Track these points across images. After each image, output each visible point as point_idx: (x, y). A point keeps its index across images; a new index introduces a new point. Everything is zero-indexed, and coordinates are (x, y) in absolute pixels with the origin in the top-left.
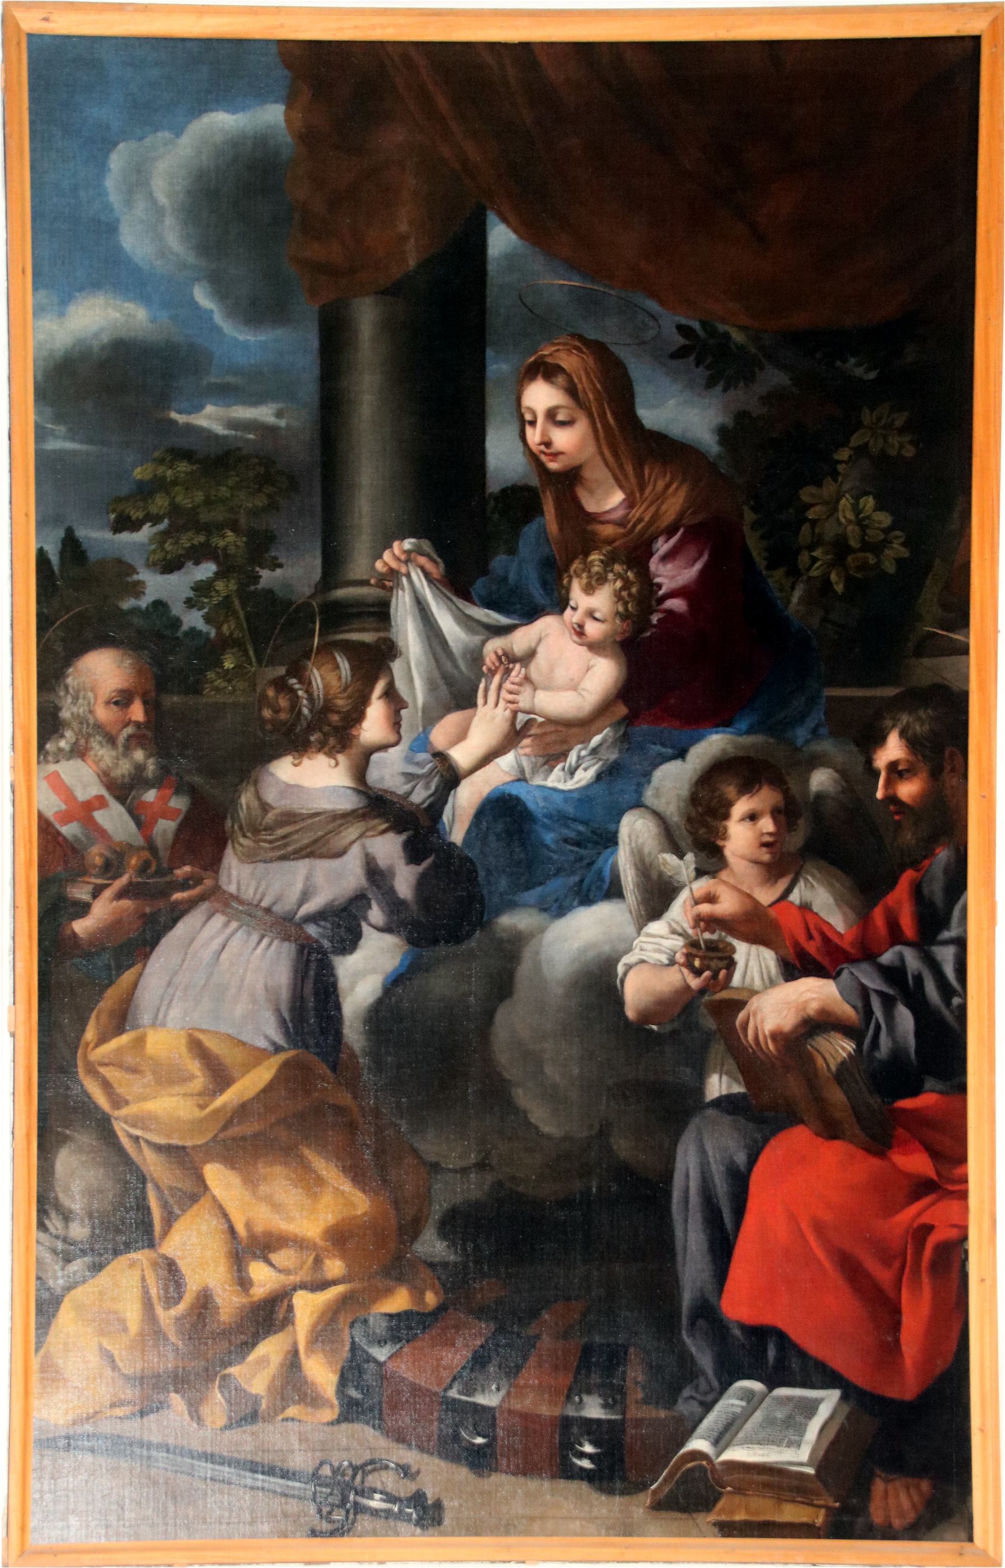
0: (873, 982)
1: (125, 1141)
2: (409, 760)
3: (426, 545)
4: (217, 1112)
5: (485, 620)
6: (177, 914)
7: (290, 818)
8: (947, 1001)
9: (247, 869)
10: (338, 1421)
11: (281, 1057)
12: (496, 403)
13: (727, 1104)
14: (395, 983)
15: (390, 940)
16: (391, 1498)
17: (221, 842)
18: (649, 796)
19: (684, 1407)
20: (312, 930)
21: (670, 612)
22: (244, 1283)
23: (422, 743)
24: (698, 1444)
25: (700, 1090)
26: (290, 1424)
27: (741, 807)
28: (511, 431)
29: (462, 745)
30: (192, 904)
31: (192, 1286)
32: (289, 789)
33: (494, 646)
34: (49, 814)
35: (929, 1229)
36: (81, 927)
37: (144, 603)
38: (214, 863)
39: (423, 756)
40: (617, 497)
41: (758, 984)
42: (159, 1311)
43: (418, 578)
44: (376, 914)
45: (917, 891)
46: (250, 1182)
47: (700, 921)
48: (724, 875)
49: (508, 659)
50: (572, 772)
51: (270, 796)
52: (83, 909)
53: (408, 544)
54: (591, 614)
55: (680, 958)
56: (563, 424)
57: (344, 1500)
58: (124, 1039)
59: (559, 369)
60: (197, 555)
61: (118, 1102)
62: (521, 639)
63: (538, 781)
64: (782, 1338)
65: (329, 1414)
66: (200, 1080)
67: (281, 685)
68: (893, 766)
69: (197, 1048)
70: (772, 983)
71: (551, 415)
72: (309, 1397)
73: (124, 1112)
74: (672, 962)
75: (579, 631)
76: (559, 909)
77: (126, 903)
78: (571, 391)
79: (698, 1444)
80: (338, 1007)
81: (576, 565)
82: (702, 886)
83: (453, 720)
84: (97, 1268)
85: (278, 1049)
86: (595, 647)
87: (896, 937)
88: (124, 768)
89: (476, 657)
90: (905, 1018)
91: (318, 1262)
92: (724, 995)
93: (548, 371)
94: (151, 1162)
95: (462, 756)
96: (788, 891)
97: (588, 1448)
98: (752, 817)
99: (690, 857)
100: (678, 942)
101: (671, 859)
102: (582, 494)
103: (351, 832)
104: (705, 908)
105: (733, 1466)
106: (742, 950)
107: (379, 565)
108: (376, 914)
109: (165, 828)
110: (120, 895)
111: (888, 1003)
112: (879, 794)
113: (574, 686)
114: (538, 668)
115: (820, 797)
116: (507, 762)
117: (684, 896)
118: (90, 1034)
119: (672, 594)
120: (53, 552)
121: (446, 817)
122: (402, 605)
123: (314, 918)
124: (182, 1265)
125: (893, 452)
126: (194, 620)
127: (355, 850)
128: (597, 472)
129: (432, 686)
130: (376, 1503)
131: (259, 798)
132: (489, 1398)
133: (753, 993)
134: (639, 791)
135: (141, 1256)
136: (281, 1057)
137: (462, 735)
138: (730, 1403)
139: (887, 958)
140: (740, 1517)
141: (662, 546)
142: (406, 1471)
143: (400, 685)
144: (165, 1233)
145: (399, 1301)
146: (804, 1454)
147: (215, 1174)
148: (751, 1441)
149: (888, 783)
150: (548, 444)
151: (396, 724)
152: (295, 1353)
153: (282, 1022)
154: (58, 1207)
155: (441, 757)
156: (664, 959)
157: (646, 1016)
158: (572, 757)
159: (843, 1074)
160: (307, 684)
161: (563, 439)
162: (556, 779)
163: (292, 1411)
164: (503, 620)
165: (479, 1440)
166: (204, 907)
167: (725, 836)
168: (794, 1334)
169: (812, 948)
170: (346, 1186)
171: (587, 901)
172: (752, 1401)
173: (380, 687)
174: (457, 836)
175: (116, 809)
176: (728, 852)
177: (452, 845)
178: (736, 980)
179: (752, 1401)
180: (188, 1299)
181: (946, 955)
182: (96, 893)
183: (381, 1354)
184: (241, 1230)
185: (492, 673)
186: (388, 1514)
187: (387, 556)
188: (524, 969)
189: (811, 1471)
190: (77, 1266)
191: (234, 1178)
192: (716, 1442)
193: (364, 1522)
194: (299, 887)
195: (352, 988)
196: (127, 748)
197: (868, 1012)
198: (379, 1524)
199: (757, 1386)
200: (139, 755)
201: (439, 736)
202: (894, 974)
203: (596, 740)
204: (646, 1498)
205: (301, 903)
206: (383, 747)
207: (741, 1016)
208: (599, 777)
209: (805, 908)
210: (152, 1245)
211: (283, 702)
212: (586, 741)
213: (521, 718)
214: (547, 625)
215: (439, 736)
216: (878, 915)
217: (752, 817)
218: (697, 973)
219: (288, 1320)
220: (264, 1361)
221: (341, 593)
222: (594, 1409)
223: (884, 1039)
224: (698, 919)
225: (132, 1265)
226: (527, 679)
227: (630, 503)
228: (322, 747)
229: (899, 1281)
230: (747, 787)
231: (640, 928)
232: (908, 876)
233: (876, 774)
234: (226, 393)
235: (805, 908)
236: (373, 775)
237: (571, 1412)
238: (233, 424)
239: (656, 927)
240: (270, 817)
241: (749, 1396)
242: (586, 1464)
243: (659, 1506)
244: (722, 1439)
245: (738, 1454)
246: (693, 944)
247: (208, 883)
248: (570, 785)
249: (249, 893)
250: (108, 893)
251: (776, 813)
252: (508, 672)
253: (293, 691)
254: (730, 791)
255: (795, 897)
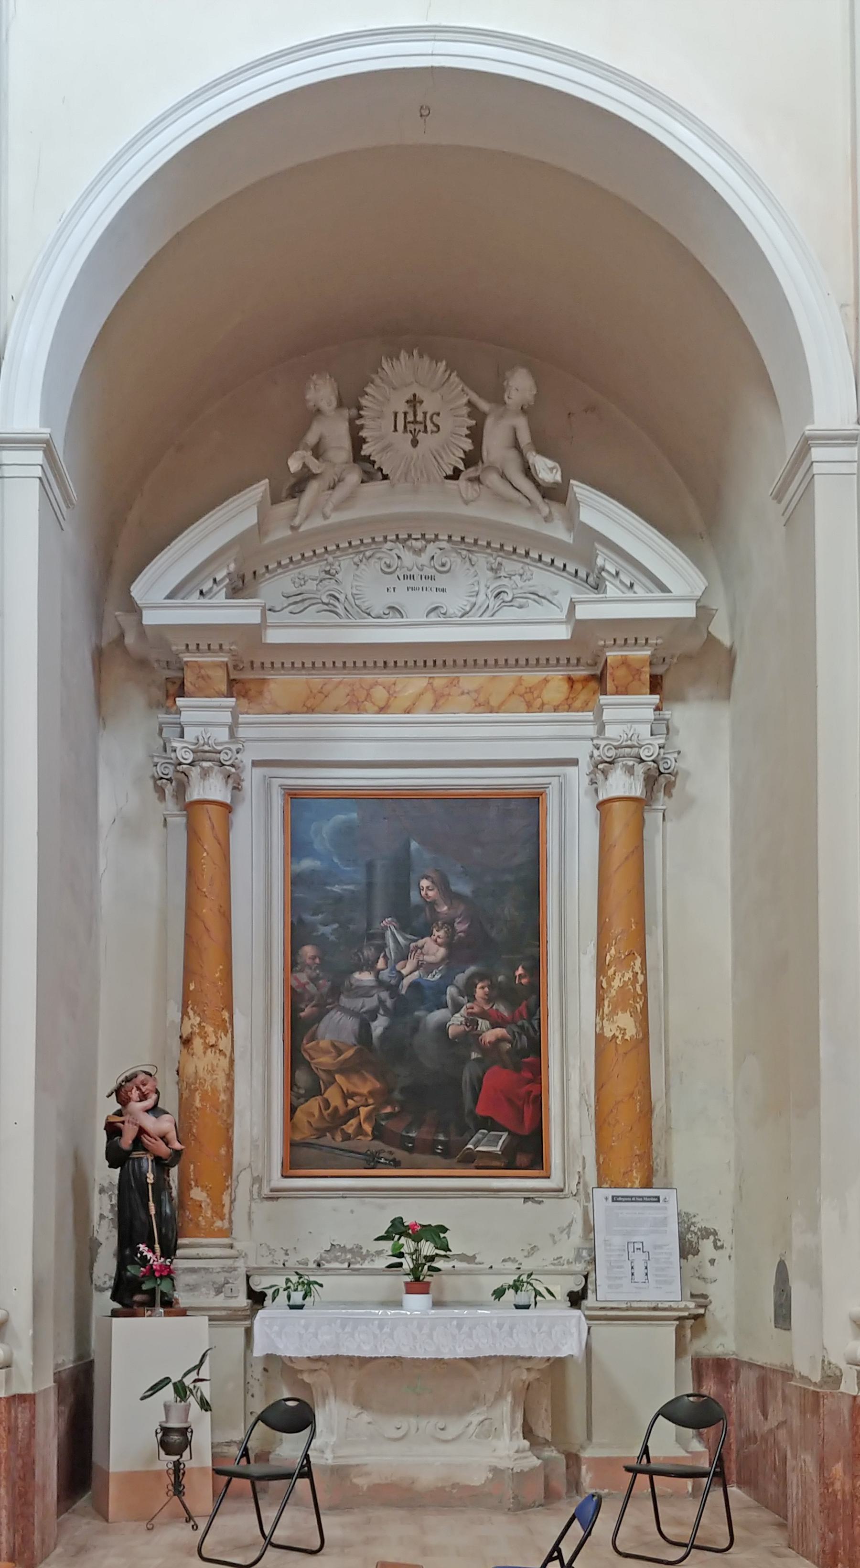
0: (516, 1030)
1: (314, 1068)
2: (389, 973)
3: (395, 920)
4: (338, 1062)
5: (40, 1436)
6: (328, 1011)
7: (358, 987)
8: (536, 1034)
9: (346, 1000)
10: (372, 1140)
11: (355, 1048)
12: (413, 886)
13: (476, 1060)
14: (386, 1029)
15: (385, 1018)
16: (386, 1160)
17: (340, 993)
18: (455, 982)
19: (467, 1135)
20: (365, 1015)
21: (460, 937)
22: (346, 1105)
23: (394, 968)
24: (470, 1146)
25: (470, 1056)
26: (324, 582)
27: (479, 985)
28: (417, 893)
29: (405, 969)
30: (332, 1009)
31: (333, 1105)
32: (358, 980)
33: (413, 945)
34: (294, 986)
35: (532, 1091)
36: (302, 1014)
37: (319, 933)
38: (338, 999)
39: (394, 972)
40: (445, 908)
41: (484, 1029)
42: (323, 1111)
43: (392, 928)
44: (381, 1012)
45: (527, 1007)
46: (348, 1079)
47: (470, 1014)
48: (475, 1002)
49: (417, 948)
50: (434, 976)
51: (353, 982)
52: (303, 1010)
53: (390, 919)
54: (439, 937)
55: (463, 1023)
56: (431, 890)
57: (374, 1159)
58: (314, 1043)
59: (430, 877)
60: (334, 922)
61: (313, 1059)
62: (420, 942)
63: (425, 978)
64: (492, 1119)
65: (370, 1138)
66: (334, 1054)
67: (356, 954)
68: (520, 975)
69: (333, 1045)
70: (488, 1030)
71: (428, 887)
72: (365, 1134)
73: (313, 1061)
74: (461, 1024)
75: (436, 941)
76: (431, 1011)
77: (314, 1008)
78: (433, 882)
79: (470, 1146)
80: (371, 1035)
81: (434, 925)
82: (469, 1005)
83: (402, 962)
84: (307, 1101)
85: (355, 1045)
86: (440, 945)
87: (522, 1018)
88: (314, 974)
89: (408, 947)
90: (524, 1038)
91: (366, 1100)
92: (475, 1032)
93: (427, 877)
94: (322, 1075)
95: (404, 972)
96: (492, 1007)
97: (440, 1147)
98: (483, 988)
99: (466, 998)
100: (463, 1019)
101: (461, 998)
102: (436, 907)
103: (374, 992)
104: (470, 1010)
105: (478, 1151)
106: (480, 1021)
107: (382, 924)
108: (381, 1012)
109: (325, 990)
110: (313, 1006)
111: (520, 1035)
112: (517, 982)
113: (434, 954)
114: (424, 950)
115: (500, 983)
116: (416, 973)
117: (465, 1007)
118: (305, 1041)
119: (461, 932)
120: (295, 922)
121: (400, 987)
122: (388, 933)
123: (365, 1013)
124: (330, 1100)
125: (442, 951)
126: (332, 938)
127: (376, 995)
128: (440, 901)
129: (396, 953)
130: (382, 1160)
131: (350, 982)
132: (413, 1135)
133: (484, 1032)
134: (452, 981)
135: (319, 1098)
136: (355, 1048)
137: (404, 967)
138: (478, 1136)
139: (520, 1023)
140: (480, 1164)
141: (458, 920)
142: (391, 1153)
143: (388, 954)
144: (325, 1091)
145: (388, 1110)
146: (498, 1148)
147: (337, 1077)
148: (483, 1145)
149: (519, 979)
150: (427, 894)
151: (386, 964)
152: (360, 1123)
153: (356, 1038)
154: (296, 1085)
155: (399, 972)
156: (459, 1023)
157: (455, 1037)
158: (434, 973)
159: (508, 1052)
160: (363, 954)
161: (430, 893)
162: (430, 978)
163: (359, 1137)
164: (415, 938)
165: (410, 1145)
166: (335, 1010)
167: (476, 992)
168: (496, 1119)
169: (500, 1021)
170: (374, 1080)
171: (438, 1009)
172: (485, 1135)
173: (382, 955)
174: (403, 992)
175: (312, 985)
176: (476, 996)
177: (402, 995)
178: (479, 1029)
179: (485, 1135)
180: (331, 1109)
181: (535, 1023)
182: (307, 1006)
183: (383, 1123)
184: (345, 1092)
185: (412, 951)
186: (386, 1164)
187: (384, 922)
188: (421, 1026)
189: (500, 1153)
190: (302, 1100)
191: (343, 1078)
192: (474, 1146)
193: (379, 1165)
194: (361, 1004)
195: (375, 1030)
196: (315, 970)
197: (514, 1036)
198: (384, 1166)
199: (485, 1131)
200: (318, 971)
201: (398, 967)
202: (522, 1027)
203: (440, 968)
204: (455, 1160)
205: (362, 1008)
206: (383, 970)
207: (480, 1038)
208: (440, 978)
209: (497, 1010)
210: (321, 1095)
211: (356, 958)
212: (438, 968)
213: (420, 962)
214: (427, 939)
215: (398, 967)
216: (517, 1012)
217: (483, 988)
218: (468, 1027)
219: (359, 1114)
220: (352, 1125)
221: (372, 931)
222: (441, 1137)
223: (519, 1043)
224: (468, 1014)
225: (316, 1099)
226: (422, 953)
227: (449, 909)
228: (367, 970)
229: (523, 1105)
230: (481, 980)
231: (453, 1015)
232: (524, 1003)
233: (516, 977)
234: (340, 882)
235: (497, 1010)
236: (380, 977)
237: (435, 1138)
238: (343, 890)
239: (457, 1015)
240: (353, 987)
241: (483, 1134)
242: (439, 1151)
243: (459, 1161)
244: (476, 1145)
245: (479, 1149)
246: (466, 1019)
247: (336, 1003)
248: (433, 979)
249: (348, 1006)
250: (309, 1007)
251: (489, 987)
252: (416, 951)
253: (358, 956)
254: (477, 981)
255: (494, 1007)
